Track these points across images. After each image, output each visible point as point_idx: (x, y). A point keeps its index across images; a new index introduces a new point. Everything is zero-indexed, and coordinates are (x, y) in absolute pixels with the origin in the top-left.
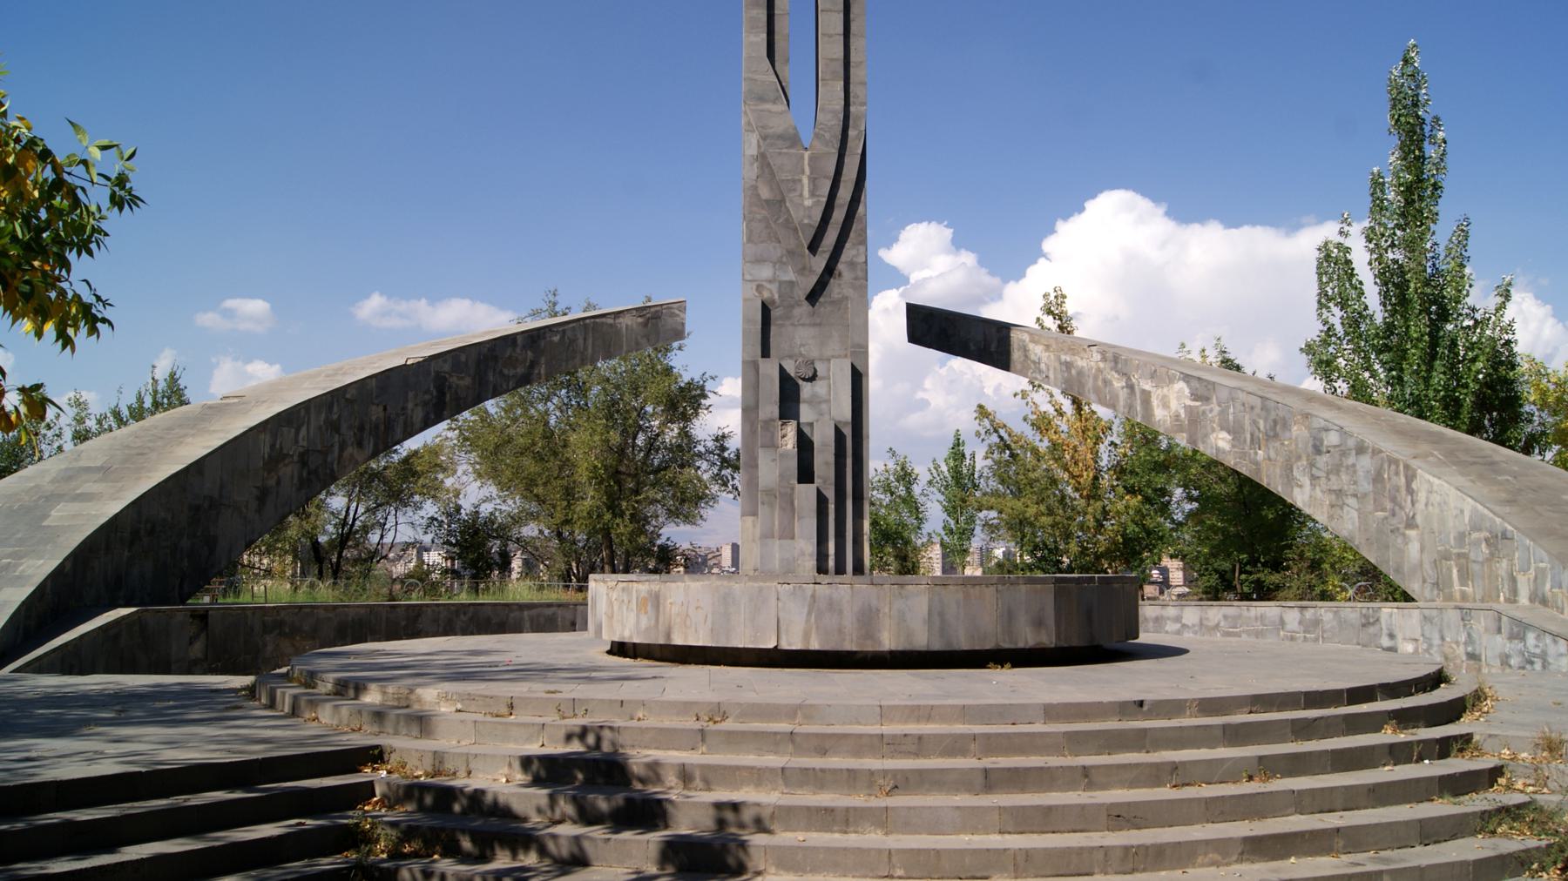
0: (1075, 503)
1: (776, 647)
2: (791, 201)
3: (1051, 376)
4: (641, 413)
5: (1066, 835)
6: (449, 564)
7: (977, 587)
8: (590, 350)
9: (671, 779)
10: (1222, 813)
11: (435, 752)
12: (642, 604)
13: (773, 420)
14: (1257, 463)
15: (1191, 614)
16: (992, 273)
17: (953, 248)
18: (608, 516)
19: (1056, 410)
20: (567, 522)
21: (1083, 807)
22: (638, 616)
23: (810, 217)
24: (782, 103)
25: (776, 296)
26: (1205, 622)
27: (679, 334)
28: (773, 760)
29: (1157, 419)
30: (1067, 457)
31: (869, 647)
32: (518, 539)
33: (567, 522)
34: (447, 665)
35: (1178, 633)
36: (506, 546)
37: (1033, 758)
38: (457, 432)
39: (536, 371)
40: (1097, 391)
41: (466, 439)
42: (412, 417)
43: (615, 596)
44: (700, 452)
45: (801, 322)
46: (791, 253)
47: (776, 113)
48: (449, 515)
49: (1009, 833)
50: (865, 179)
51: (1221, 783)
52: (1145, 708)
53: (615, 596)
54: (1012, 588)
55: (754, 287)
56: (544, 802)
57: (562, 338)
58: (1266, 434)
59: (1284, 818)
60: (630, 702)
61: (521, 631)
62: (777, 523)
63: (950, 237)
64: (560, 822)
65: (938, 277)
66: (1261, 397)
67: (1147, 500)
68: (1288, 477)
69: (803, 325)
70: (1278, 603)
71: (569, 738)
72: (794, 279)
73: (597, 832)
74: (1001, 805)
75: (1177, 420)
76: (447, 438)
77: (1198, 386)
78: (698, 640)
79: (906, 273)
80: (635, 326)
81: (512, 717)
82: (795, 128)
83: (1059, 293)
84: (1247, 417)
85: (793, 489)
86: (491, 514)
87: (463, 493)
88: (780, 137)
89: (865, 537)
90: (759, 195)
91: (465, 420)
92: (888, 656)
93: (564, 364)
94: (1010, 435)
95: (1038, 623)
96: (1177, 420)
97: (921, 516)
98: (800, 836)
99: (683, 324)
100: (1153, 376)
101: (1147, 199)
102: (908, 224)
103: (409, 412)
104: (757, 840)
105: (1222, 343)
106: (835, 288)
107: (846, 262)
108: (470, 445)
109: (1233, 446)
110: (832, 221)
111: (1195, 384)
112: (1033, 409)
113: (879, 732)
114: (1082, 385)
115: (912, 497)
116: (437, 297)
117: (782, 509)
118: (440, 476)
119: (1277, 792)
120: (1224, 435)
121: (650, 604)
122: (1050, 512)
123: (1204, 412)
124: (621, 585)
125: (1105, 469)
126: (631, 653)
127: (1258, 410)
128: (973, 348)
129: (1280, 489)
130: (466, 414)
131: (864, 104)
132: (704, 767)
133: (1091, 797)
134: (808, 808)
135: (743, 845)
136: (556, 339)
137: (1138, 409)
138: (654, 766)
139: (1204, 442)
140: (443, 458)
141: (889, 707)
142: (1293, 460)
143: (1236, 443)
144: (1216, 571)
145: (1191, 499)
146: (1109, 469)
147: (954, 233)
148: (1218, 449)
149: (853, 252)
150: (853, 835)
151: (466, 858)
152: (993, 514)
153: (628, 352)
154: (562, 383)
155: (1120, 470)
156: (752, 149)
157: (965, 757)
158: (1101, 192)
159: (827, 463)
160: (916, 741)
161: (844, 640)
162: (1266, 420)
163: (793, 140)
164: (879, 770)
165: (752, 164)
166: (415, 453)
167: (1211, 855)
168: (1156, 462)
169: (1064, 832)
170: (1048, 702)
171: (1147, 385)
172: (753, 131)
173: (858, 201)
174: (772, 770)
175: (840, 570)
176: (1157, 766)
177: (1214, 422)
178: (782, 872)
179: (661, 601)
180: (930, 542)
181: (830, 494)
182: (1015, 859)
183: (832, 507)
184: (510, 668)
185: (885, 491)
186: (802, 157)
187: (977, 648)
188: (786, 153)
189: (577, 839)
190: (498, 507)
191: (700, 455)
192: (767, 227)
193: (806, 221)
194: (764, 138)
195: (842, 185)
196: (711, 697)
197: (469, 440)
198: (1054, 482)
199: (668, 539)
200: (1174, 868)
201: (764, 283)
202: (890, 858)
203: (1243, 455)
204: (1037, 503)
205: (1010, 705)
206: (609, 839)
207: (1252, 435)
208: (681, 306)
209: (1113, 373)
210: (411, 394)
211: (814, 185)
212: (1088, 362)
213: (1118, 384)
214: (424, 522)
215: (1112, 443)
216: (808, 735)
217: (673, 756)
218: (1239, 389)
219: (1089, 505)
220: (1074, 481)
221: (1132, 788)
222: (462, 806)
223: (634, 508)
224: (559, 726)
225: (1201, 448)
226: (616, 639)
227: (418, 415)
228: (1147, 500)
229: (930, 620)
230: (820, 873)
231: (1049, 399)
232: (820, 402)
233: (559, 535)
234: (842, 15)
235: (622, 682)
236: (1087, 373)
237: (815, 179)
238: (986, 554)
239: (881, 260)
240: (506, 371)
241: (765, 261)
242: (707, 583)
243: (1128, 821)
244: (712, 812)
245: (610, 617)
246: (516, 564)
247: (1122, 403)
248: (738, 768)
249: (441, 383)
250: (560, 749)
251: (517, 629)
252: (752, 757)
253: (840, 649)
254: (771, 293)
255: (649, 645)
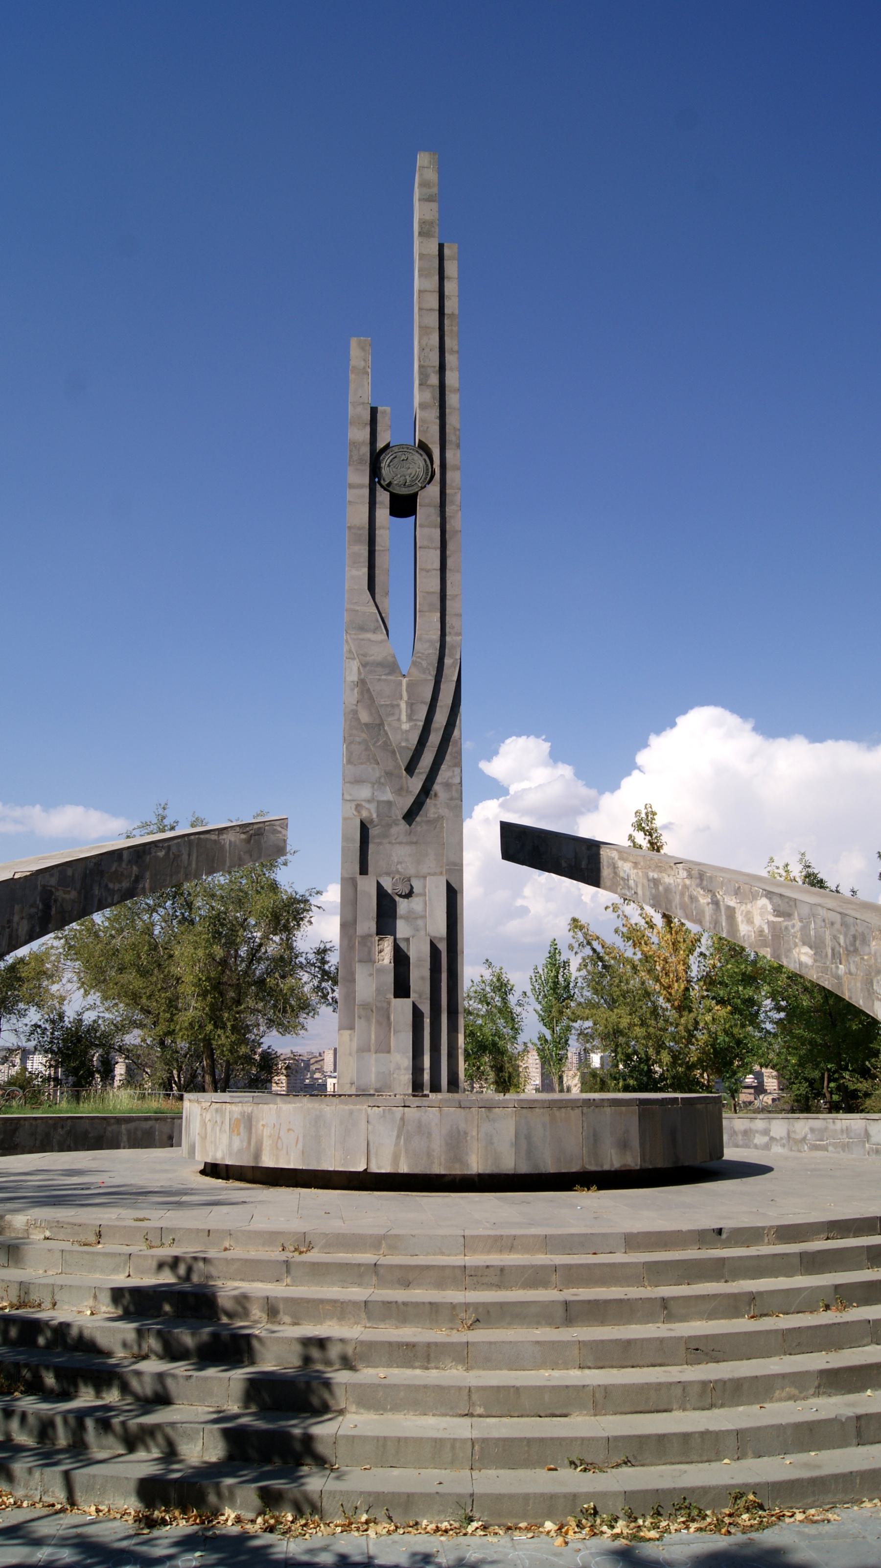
0: (668, 1013)
1: (366, 1170)
2: (389, 725)
3: (640, 892)
4: (244, 925)
5: (645, 1369)
6: (52, 1073)
7: (563, 1110)
8: (194, 865)
9: (257, 1313)
10: (799, 1344)
11: (21, 1283)
12: (234, 1128)
13: (370, 936)
14: (838, 978)
15: (779, 1126)
16: (589, 785)
17: (551, 761)
18: (210, 1027)
19: (647, 923)
20: (170, 1033)
21: (661, 1340)
22: (230, 1138)
23: (407, 740)
24: (382, 633)
25: (375, 816)
26: (792, 1135)
27: (281, 850)
28: (357, 1293)
29: (742, 934)
30: (658, 968)
31: (457, 1170)
32: (120, 1047)
33: (170, 1033)
34: (39, 1186)
35: (767, 1147)
36: (108, 1053)
37: (613, 1289)
38: (63, 941)
39: (141, 886)
40: (683, 907)
41: (71, 947)
42: (17, 930)
43: (208, 1117)
44: (301, 963)
45: (398, 840)
46: (389, 774)
47: (375, 642)
48: (53, 1022)
49: (589, 1368)
50: (460, 705)
51: (798, 1313)
52: (724, 1236)
53: (208, 1117)
54: (597, 1110)
55: (353, 807)
56: (131, 1336)
57: (167, 854)
58: (846, 949)
59: (860, 1348)
60: (217, 1231)
61: (118, 1147)
62: (373, 1037)
63: (548, 750)
64: (145, 1357)
65: (536, 788)
66: (840, 913)
67: (736, 1010)
68: (869, 991)
69: (400, 843)
70: (863, 1115)
71: (161, 1266)
72: (391, 799)
73: (180, 1368)
74: (581, 1339)
75: (761, 936)
76: (52, 947)
77: (780, 902)
78: (289, 1163)
79: (505, 784)
80: (238, 842)
81: (100, 1246)
82: (394, 657)
83: (650, 809)
84: (828, 933)
85: (389, 1003)
86: (95, 1021)
87: (68, 998)
88: (380, 664)
89: (460, 1051)
90: (358, 719)
91: (71, 930)
92: (476, 1179)
93: (168, 878)
94: (603, 947)
95: (623, 1145)
96: (761, 936)
97: (516, 1026)
98: (382, 1372)
99: (285, 841)
100: (737, 892)
101: (735, 716)
102: (507, 738)
103: (15, 925)
104: (340, 1377)
105: (807, 858)
106: (431, 808)
107: (442, 783)
108: (76, 954)
109: (815, 961)
110: (428, 744)
111: (777, 900)
112: (624, 923)
113: (462, 1263)
114: (669, 901)
115: (508, 1007)
116: (51, 803)
117: (379, 1023)
118: (45, 983)
119: (853, 1322)
120: (806, 949)
121: (242, 1126)
122: (643, 1024)
123: (786, 928)
124: (215, 1106)
125: (695, 980)
126: (224, 1174)
127: (838, 926)
128: (564, 865)
129: (861, 1002)
130: (74, 925)
131: (459, 634)
132: (287, 1300)
133: (671, 1330)
134: (390, 1344)
135: (327, 1384)
136: (161, 854)
137: (724, 924)
138: (243, 1300)
139: (787, 957)
140: (48, 966)
141: (472, 1237)
142: (873, 974)
143: (818, 958)
144: (806, 1079)
145: (779, 1009)
146: (699, 980)
147: (551, 747)
148: (801, 964)
149: (449, 774)
150: (434, 1371)
151: (48, 1395)
152: (589, 1024)
153: (230, 867)
154: (168, 894)
155: (709, 981)
156: (353, 677)
157: (546, 1289)
158: (692, 708)
159: (423, 978)
160: (499, 1273)
161: (433, 1163)
162: (846, 936)
163: (392, 667)
164: (460, 1304)
165: (353, 690)
166: (21, 961)
167: (787, 1389)
168: (744, 974)
169: (644, 1366)
170: (628, 1231)
171: (731, 902)
172: (353, 659)
173: (454, 725)
174: (355, 1303)
175: (435, 1088)
176: (735, 1298)
177: (796, 937)
178: (362, 1411)
179: (254, 1123)
180: (526, 1050)
181: (426, 1008)
182: (594, 1396)
183: (427, 1021)
184: (101, 1191)
185: (481, 1002)
186: (400, 683)
187: (563, 1171)
188: (385, 680)
189: (160, 1377)
190: (102, 1015)
191: (301, 966)
192: (367, 749)
193: (403, 744)
194: (364, 665)
195: (438, 710)
196: (296, 1225)
197: (72, 950)
198: (647, 994)
199: (269, 1047)
200: (752, 1404)
201: (364, 804)
202: (469, 1396)
203: (825, 970)
204: (630, 1014)
205: (592, 1234)
206: (190, 1376)
207: (833, 950)
208: (284, 823)
209: (699, 889)
210: (17, 908)
211: (412, 710)
212: (675, 879)
213: (704, 900)
214: (28, 1029)
215: (702, 954)
216: (391, 1267)
217: (258, 1288)
218: (820, 905)
219: (681, 1016)
220: (665, 992)
221: (711, 1319)
222: (47, 1339)
223: (236, 1019)
224: (145, 1257)
225: (785, 963)
226: (209, 1161)
227: (23, 928)
228: (736, 1010)
229: (516, 1144)
230: (400, 1411)
231: (639, 912)
232: (416, 918)
233: (162, 1043)
234: (438, 552)
235: (211, 1207)
236: (674, 889)
237: (412, 704)
238: (584, 1060)
239: (481, 772)
240: (111, 886)
241: (364, 782)
242: (298, 1105)
243: (707, 1354)
244: (298, 1348)
245: (204, 1138)
246: (120, 1070)
247: (707, 918)
248: (322, 1301)
249: (47, 897)
250: (149, 1280)
251: (114, 1144)
252: (336, 1289)
253: (428, 1172)
254: (370, 812)
255: (241, 1167)
